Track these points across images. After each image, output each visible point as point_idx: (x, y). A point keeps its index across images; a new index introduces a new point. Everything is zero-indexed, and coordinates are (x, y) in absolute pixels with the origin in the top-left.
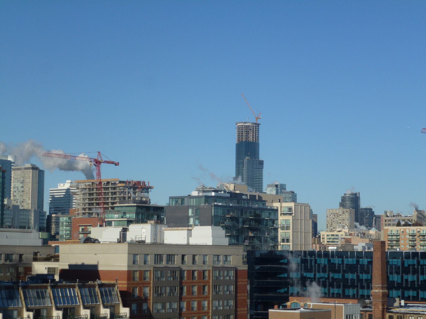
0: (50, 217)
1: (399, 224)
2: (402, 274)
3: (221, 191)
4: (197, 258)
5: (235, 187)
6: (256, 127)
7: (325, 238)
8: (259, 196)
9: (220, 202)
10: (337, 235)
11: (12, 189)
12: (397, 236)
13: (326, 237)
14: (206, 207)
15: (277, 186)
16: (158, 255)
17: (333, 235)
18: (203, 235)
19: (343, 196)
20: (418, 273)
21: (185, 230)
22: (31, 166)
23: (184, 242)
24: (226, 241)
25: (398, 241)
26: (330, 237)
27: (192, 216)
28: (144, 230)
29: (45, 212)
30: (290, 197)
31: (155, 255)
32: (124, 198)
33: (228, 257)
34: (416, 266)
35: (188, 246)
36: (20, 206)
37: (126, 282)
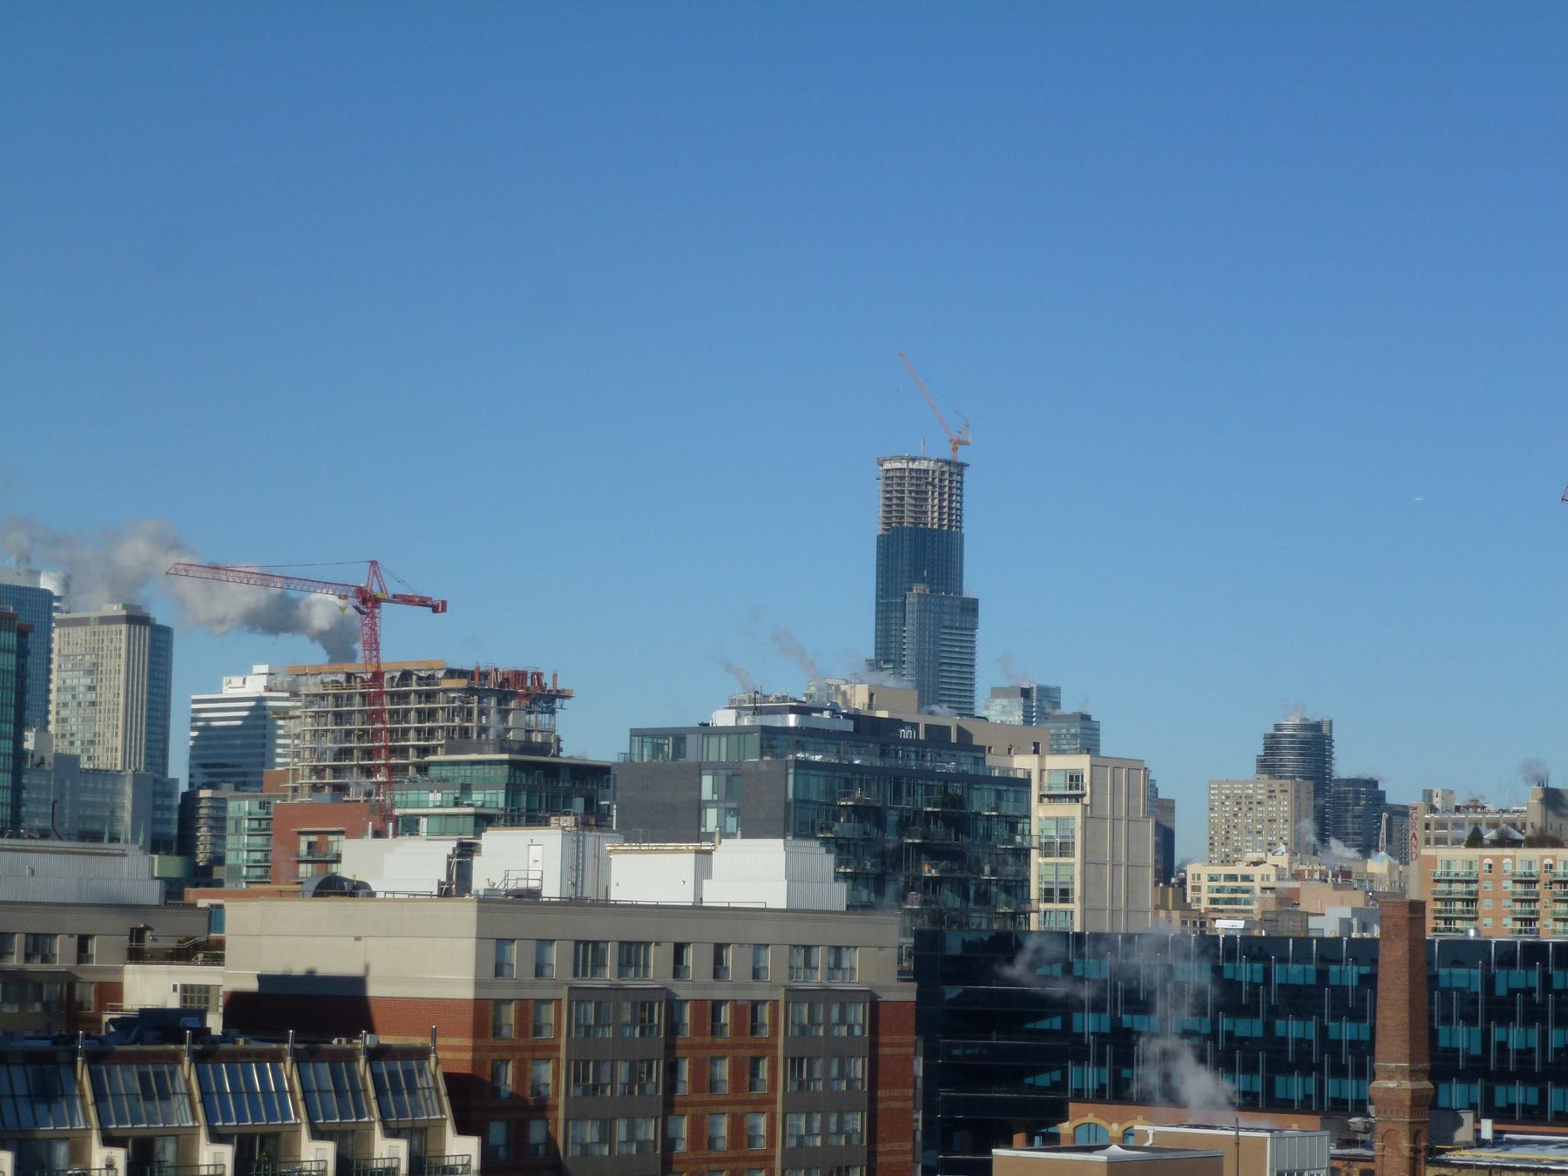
0: (190, 799)
1: (1475, 840)
2: (1487, 1021)
3: (821, 710)
4: (729, 955)
5: (871, 696)
6: (951, 474)
7: (1204, 889)
8: (959, 728)
9: (816, 752)
10: (1246, 878)
11: (53, 697)
12: (1467, 882)
13: (1205, 884)
14: (763, 768)
15: (1026, 693)
16: (586, 943)
17: (1233, 878)
18: (754, 873)
19: (1272, 731)
20: (1544, 1021)
21: (688, 851)
22: (124, 613)
23: (685, 897)
24: (837, 895)
25: (1471, 900)
26: (1222, 883)
27: (712, 801)
28: (535, 851)
29: (176, 781)
30: (1075, 736)
31: (577, 943)
32: (465, 732)
33: (845, 955)
34: (1537, 996)
35: (697, 910)
36: (84, 759)
37: (468, 1042)
